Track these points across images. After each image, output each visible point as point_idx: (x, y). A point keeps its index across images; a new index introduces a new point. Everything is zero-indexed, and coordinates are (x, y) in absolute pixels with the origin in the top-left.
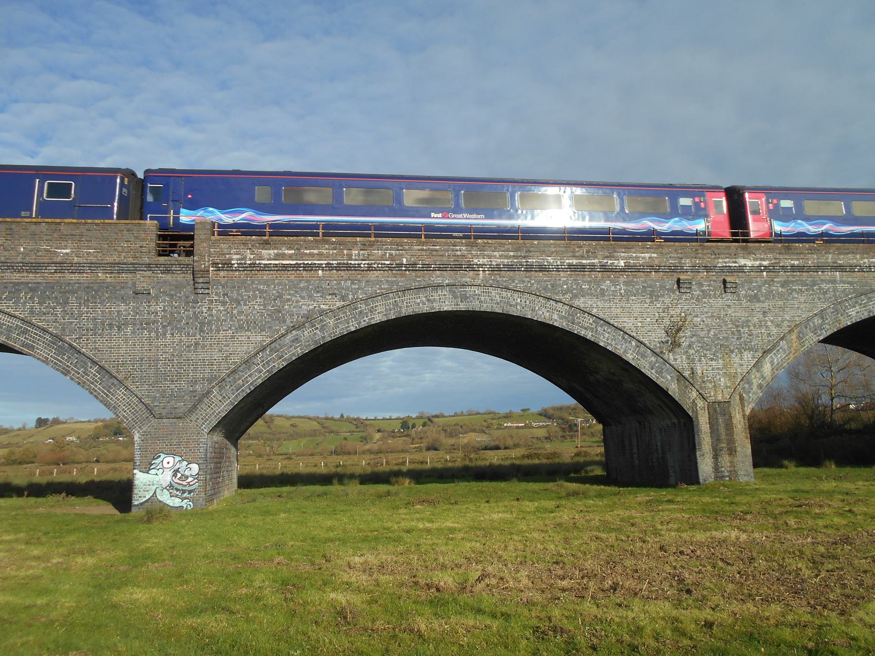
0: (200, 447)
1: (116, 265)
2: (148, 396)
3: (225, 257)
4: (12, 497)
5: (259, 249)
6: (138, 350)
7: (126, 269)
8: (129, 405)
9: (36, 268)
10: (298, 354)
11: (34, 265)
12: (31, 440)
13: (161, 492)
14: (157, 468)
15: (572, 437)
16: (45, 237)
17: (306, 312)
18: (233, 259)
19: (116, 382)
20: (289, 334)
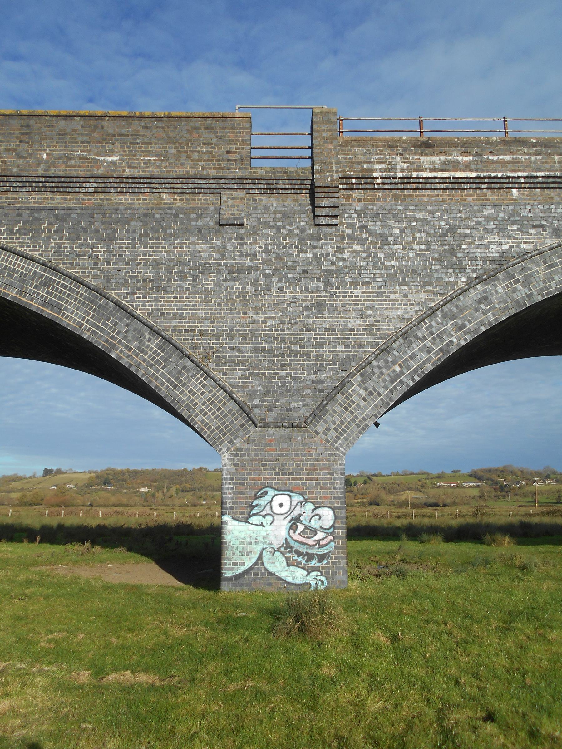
0: (335, 479)
1: (190, 181)
2: (242, 389)
3: (363, 167)
4: (22, 541)
5: (415, 153)
6: (225, 313)
7: (205, 186)
8: (212, 403)
9: (65, 185)
10: (490, 323)
11: (63, 180)
12: (40, 486)
13: (271, 556)
14: (264, 513)
15: (504, 497)
16: (80, 139)
17: (497, 255)
18: (375, 171)
19: (189, 363)
20: (472, 291)
